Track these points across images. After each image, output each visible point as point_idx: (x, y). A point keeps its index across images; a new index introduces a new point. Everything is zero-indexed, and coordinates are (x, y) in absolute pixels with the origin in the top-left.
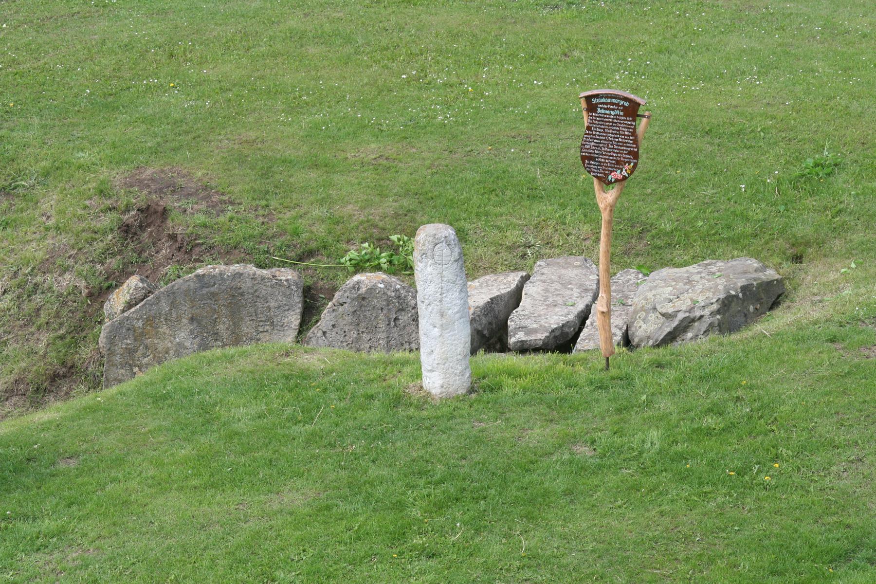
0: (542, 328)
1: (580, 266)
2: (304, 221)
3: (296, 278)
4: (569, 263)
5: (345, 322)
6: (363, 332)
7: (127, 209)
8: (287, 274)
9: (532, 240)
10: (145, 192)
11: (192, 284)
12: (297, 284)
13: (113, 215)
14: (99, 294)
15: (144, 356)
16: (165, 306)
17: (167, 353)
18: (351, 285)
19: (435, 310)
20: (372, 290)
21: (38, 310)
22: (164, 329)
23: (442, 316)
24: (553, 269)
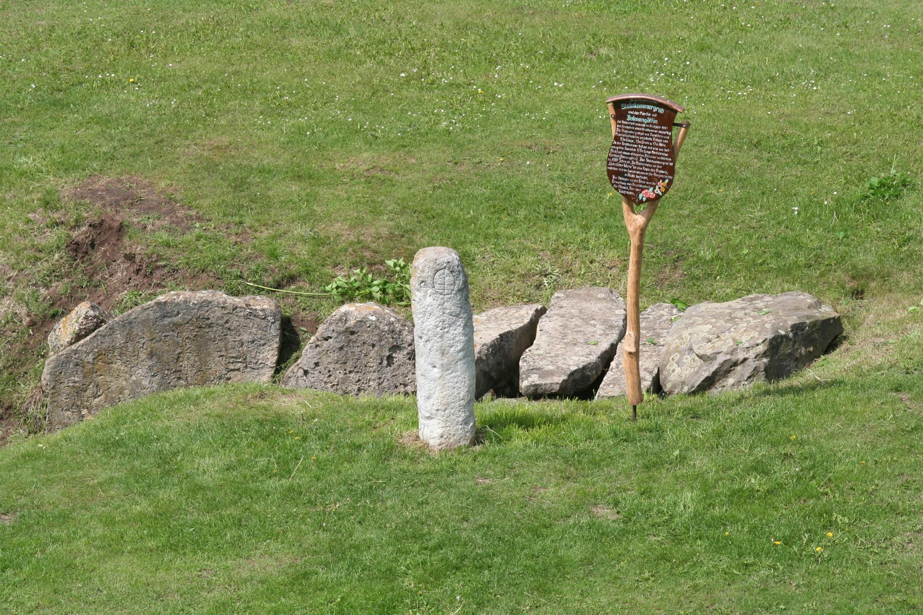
0: (559, 370)
3: (273, 308)
5: (330, 360)
6: (350, 372)
7: (77, 225)
8: (263, 304)
11: (151, 313)
12: (274, 316)
13: (61, 231)
16: (119, 339)
17: (121, 393)
18: (337, 317)
20: (362, 322)
22: (118, 365)
23: (443, 354)
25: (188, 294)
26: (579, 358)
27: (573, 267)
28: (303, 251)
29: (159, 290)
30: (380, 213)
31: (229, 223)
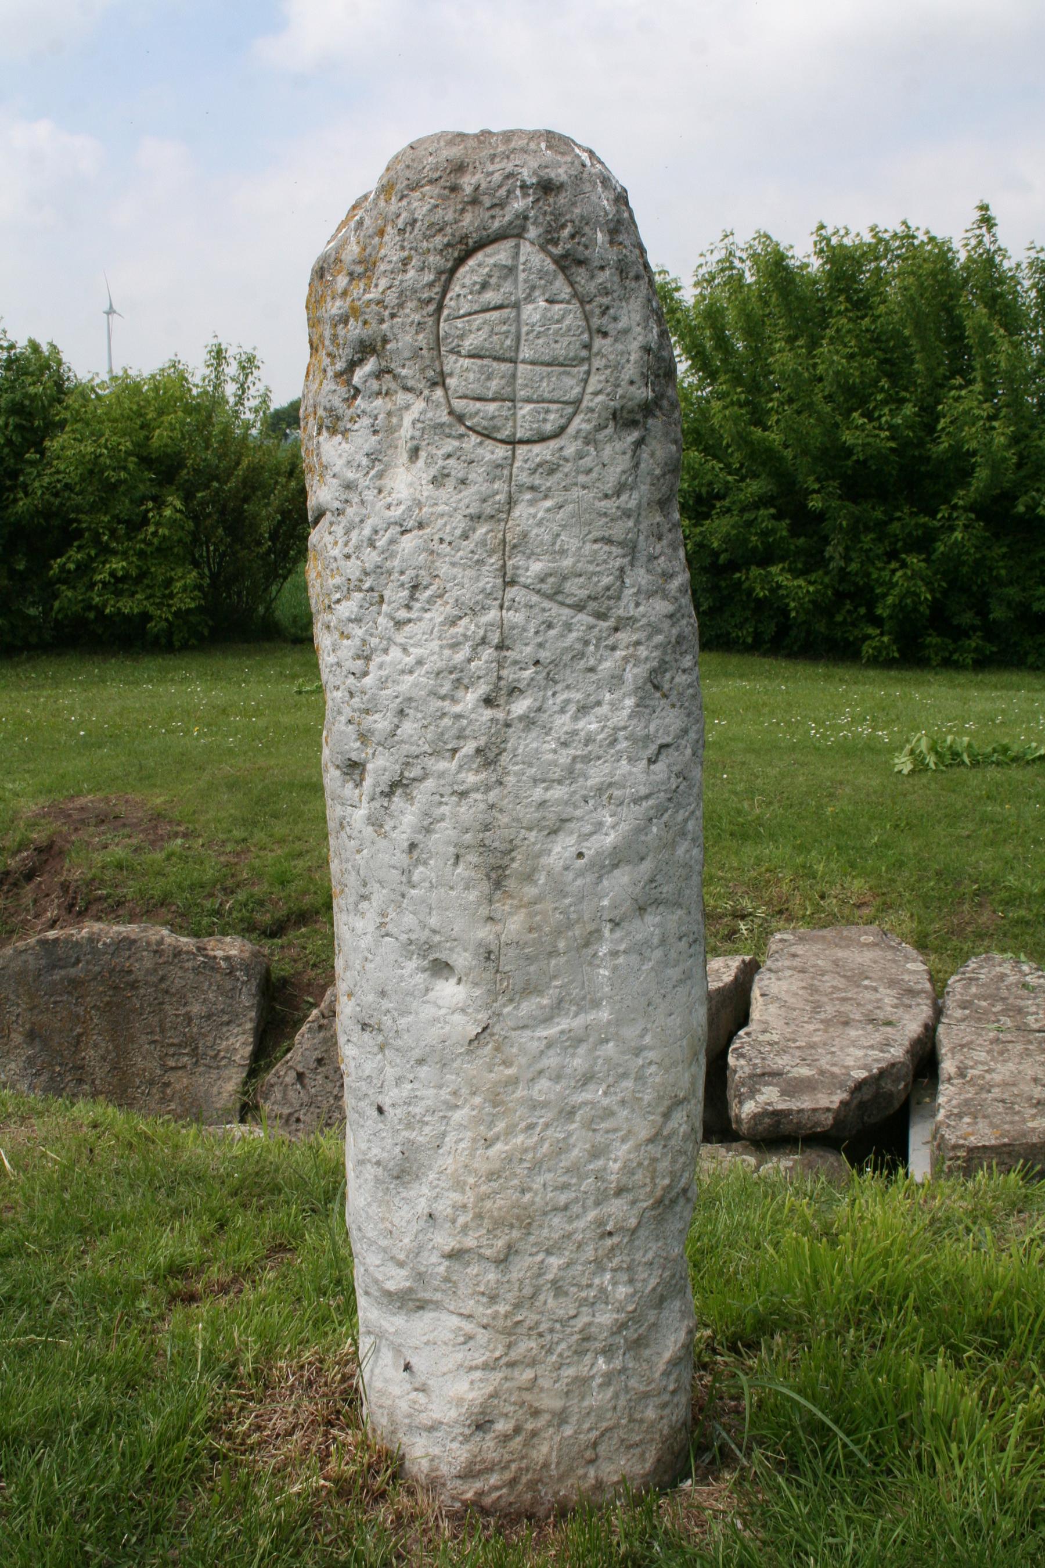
0: (830, 1081)
1: (875, 945)
2: (300, 863)
4: (850, 939)
8: (232, 947)
9: (747, 904)
11: (31, 959)
19: (445, 832)
23: (497, 877)
24: (817, 948)
26: (862, 1054)
27: (790, 905)
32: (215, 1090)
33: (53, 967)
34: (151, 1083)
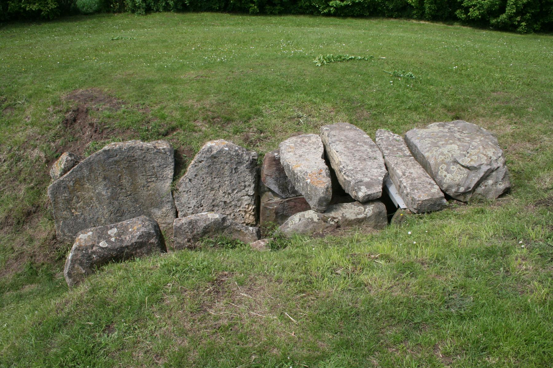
3: (169, 147)
5: (203, 173)
6: (215, 178)
7: (68, 111)
8: (163, 145)
10: (77, 101)
11: (101, 156)
12: (170, 151)
13: (61, 114)
14: (50, 162)
15: (78, 203)
16: (86, 172)
17: (91, 199)
18: (206, 149)
20: (220, 152)
21: (20, 171)
22: (87, 185)
25: (121, 144)
28: (177, 114)
29: (107, 140)
30: (209, 94)
31: (138, 104)
32: (163, 186)
33: (109, 158)
34: (144, 186)
